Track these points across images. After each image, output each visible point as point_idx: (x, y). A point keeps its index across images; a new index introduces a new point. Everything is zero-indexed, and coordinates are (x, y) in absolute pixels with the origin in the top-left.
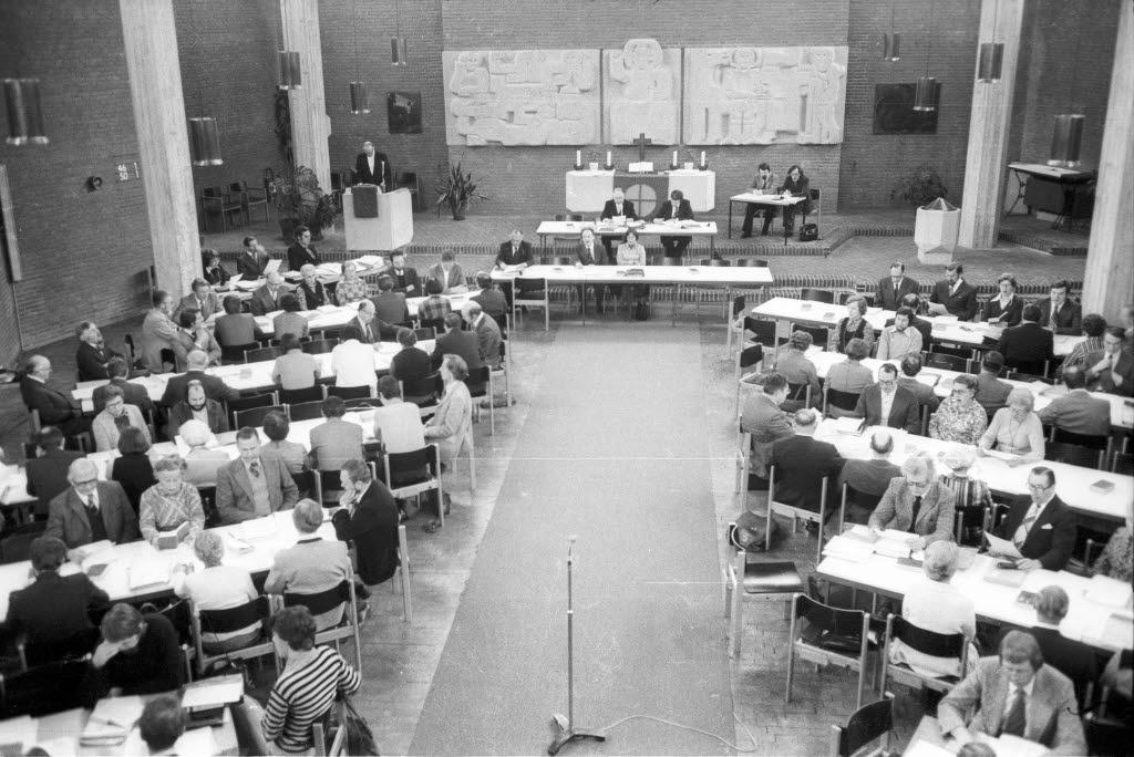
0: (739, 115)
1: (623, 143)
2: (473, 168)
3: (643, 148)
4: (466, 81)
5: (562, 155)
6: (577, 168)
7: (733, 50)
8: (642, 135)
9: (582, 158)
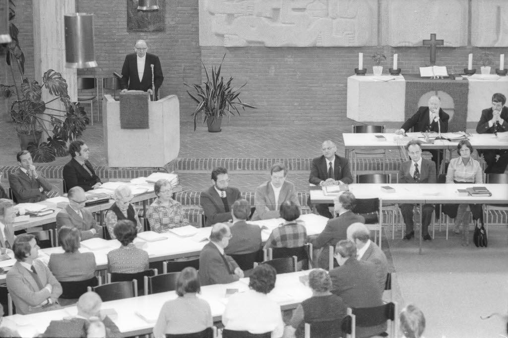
1: (403, 45)
2: (235, 75)
3: (433, 50)
5: (346, 59)
6: (357, 72)
9: (364, 61)
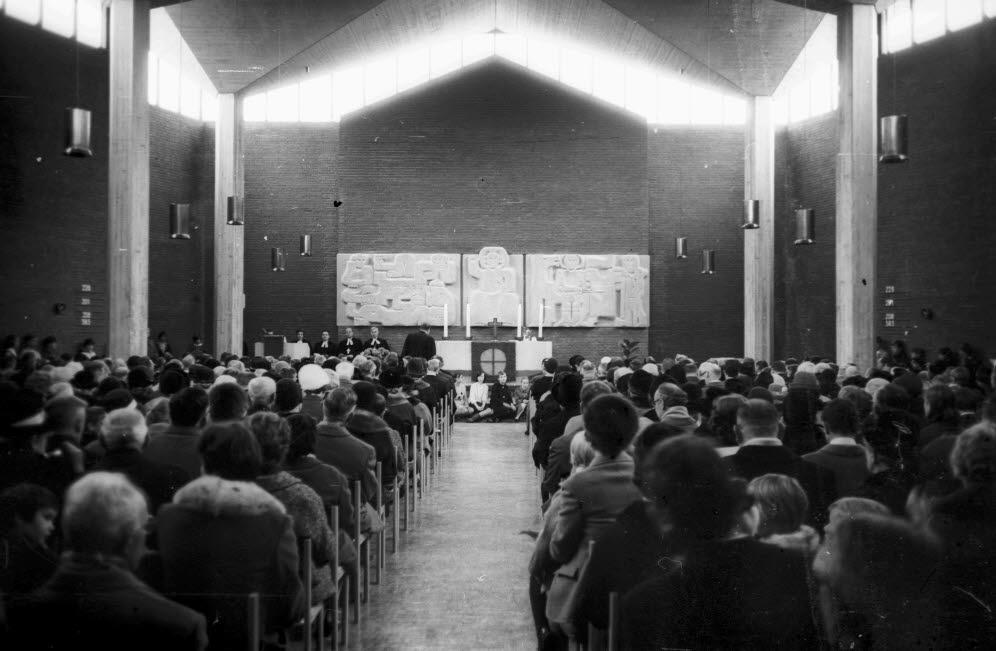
0: (569, 304)
4: (355, 276)
7: (563, 255)
8: (495, 319)
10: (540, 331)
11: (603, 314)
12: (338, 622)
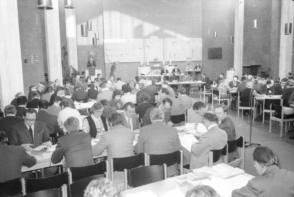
10: (170, 62)
11: (189, 57)
12: (130, 178)
